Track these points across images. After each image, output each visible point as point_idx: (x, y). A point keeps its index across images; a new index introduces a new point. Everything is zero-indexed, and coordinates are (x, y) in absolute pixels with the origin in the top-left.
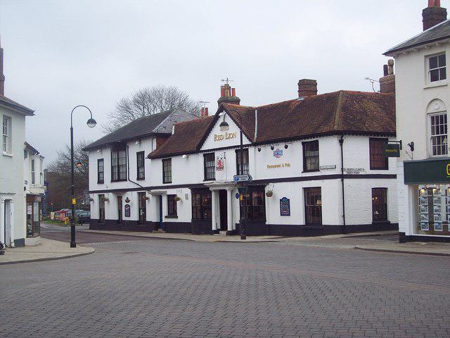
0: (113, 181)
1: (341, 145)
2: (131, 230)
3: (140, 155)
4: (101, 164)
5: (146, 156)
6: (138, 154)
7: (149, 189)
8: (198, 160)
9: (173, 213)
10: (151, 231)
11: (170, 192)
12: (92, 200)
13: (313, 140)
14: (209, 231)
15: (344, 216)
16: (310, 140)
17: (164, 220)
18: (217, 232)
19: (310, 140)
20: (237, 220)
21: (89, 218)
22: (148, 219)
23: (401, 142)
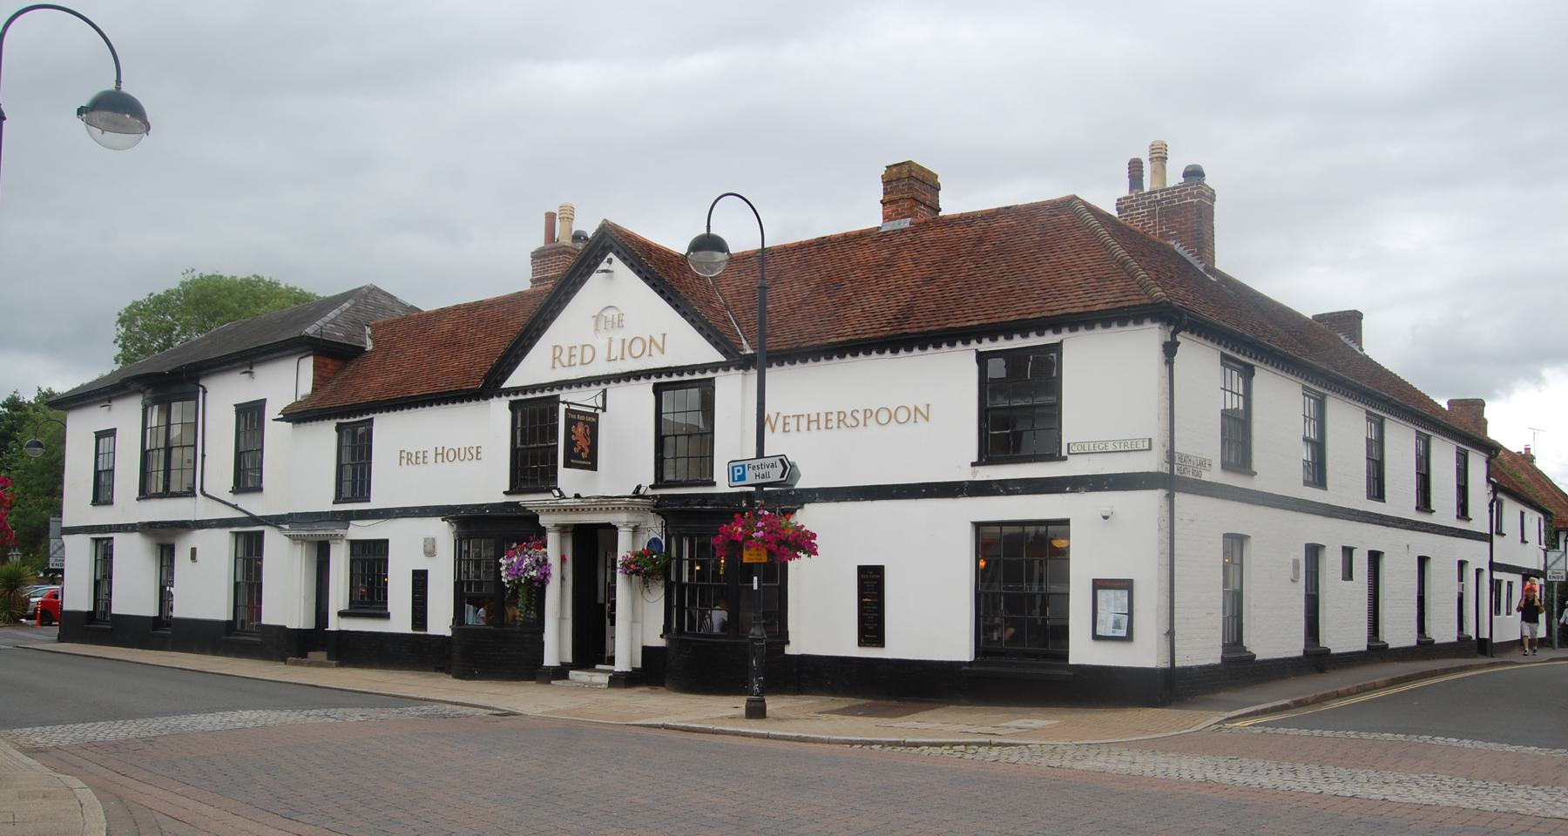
0: (144, 494)
1: (1169, 362)
3: (250, 415)
4: (105, 442)
5: (272, 411)
7: (276, 521)
9: (369, 595)
12: (1201, 263)
13: (1034, 340)
15: (1171, 634)
17: (335, 624)
18: (561, 672)
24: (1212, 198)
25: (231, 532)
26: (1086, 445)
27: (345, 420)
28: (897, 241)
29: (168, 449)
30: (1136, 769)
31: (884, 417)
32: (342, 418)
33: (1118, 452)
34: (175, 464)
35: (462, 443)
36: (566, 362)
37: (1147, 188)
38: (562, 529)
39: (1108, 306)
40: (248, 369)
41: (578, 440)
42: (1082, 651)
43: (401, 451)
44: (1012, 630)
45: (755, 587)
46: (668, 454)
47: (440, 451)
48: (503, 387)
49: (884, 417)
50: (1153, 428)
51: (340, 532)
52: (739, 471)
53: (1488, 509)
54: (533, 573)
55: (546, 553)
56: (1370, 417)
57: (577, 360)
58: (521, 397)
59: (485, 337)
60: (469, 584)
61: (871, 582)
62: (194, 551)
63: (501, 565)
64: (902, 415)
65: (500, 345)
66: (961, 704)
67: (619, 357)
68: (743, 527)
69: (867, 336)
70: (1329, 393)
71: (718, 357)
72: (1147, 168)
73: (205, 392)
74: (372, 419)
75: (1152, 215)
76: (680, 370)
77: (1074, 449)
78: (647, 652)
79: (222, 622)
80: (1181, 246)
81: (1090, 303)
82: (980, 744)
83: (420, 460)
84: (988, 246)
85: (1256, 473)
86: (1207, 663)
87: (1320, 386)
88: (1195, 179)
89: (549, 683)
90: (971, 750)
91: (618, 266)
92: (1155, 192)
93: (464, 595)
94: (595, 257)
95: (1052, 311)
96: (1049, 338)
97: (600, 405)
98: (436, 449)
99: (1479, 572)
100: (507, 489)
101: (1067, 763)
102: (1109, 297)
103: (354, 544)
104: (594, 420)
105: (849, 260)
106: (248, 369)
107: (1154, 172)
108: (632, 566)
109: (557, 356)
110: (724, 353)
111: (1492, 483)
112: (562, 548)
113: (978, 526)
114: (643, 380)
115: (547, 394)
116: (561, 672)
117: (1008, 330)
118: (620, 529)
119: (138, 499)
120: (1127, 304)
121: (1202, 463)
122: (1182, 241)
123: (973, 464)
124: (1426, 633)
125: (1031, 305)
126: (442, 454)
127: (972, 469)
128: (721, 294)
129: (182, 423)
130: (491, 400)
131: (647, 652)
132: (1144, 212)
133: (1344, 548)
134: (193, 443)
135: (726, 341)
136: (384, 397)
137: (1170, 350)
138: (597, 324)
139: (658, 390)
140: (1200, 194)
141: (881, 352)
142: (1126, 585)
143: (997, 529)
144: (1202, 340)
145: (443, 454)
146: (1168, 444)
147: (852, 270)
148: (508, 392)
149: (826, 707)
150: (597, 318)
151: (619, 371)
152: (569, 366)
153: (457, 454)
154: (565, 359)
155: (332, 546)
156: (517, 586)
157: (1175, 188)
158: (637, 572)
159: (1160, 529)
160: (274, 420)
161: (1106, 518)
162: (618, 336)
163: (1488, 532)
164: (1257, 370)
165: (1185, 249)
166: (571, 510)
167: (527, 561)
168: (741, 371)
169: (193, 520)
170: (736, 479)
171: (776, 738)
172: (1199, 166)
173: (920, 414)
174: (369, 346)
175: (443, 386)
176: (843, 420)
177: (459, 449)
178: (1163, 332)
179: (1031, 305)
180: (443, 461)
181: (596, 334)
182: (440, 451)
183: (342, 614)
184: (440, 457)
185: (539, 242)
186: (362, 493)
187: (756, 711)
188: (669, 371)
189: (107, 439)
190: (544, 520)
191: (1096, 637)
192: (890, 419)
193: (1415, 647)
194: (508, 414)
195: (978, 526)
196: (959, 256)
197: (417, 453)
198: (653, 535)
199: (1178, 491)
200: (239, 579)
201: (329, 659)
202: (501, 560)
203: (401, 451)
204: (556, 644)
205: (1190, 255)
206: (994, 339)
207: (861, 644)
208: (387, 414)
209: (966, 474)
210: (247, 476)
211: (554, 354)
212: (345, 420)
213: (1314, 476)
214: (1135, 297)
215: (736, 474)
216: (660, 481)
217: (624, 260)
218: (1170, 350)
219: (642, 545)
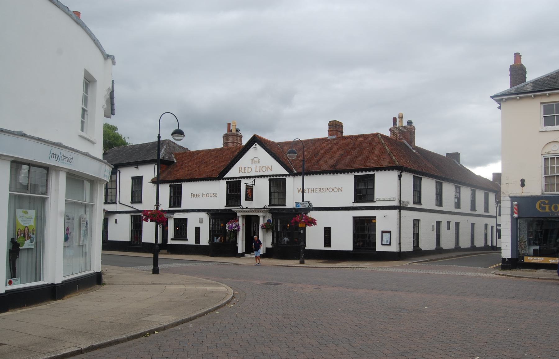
1: (400, 180)
2: (125, 250)
3: (137, 181)
8: (221, 187)
11: (177, 216)
13: (368, 173)
14: (232, 252)
15: (400, 244)
17: (169, 242)
18: (242, 255)
24: (414, 129)
25: (130, 215)
26: (380, 199)
27: (172, 184)
28: (332, 142)
30: (389, 271)
31: (331, 190)
32: (172, 183)
35: (211, 192)
36: (243, 171)
37: (397, 126)
38: (243, 217)
39: (386, 166)
40: (136, 167)
42: (379, 248)
43: (191, 194)
44: (362, 243)
45: (302, 233)
46: (273, 197)
48: (224, 177)
49: (331, 190)
50: (396, 196)
51: (172, 216)
53: (496, 209)
54: (236, 228)
55: (238, 223)
56: (456, 187)
57: (246, 171)
58: (229, 180)
59: (214, 161)
60: (215, 231)
61: (327, 231)
63: (226, 226)
64: (335, 190)
66: (350, 261)
67: (259, 171)
68: (299, 218)
69: (327, 170)
70: (444, 182)
71: (287, 173)
72: (398, 120)
73: (120, 172)
75: (399, 133)
77: (377, 200)
78: (267, 249)
79: (127, 242)
81: (381, 165)
82: (357, 267)
83: (198, 196)
84: (356, 146)
86: (409, 251)
87: (441, 180)
88: (410, 124)
89: (240, 257)
90: (355, 268)
91: (258, 146)
92: (400, 127)
93: (213, 234)
95: (372, 166)
96: (372, 173)
98: (203, 193)
99: (492, 227)
100: (226, 205)
101: (375, 270)
102: (386, 164)
104: (252, 188)
105: (320, 147)
106: (136, 167)
107: (399, 121)
108: (265, 227)
110: (288, 172)
111: (497, 201)
112: (243, 222)
113: (354, 218)
114: (266, 178)
117: (362, 170)
120: (390, 166)
121: (408, 203)
123: (353, 203)
124: (474, 244)
125: (367, 164)
126: (204, 195)
127: (353, 204)
128: (285, 154)
130: (220, 181)
131: (267, 249)
133: (447, 222)
134: (115, 187)
135: (289, 169)
136: (186, 178)
137: (400, 177)
138: (252, 161)
139: (270, 180)
140: (411, 129)
141: (330, 174)
142: (389, 232)
143: (359, 218)
144: (408, 173)
145: (205, 195)
146: (399, 199)
147: (321, 150)
148: (226, 179)
149: (317, 262)
150: (252, 160)
151: (259, 175)
152: (244, 172)
153: (209, 195)
155: (168, 220)
156: (231, 231)
157: (405, 126)
158: (265, 228)
159: (397, 219)
161: (385, 216)
162: (258, 165)
163: (495, 215)
164: (422, 178)
166: (247, 212)
167: (234, 225)
168: (293, 177)
169: (116, 211)
171: (310, 267)
172: (411, 121)
173: (340, 190)
174: (175, 161)
175: (204, 176)
178: (398, 172)
179: (367, 164)
183: (172, 239)
184: (204, 196)
185: (226, 132)
186: (178, 203)
187: (302, 262)
188: (273, 176)
190: (238, 214)
191: (382, 244)
192: (332, 191)
193: (470, 248)
194: (226, 184)
195: (354, 218)
196: (349, 148)
198: (269, 218)
199: (402, 210)
200: (132, 229)
201: (168, 252)
202: (226, 225)
203: (191, 194)
204: (241, 246)
206: (358, 172)
207: (325, 247)
208: (187, 183)
209: (351, 205)
210: (136, 197)
212: (172, 184)
213: (439, 203)
214: (392, 164)
215: (297, 206)
216: (270, 204)
217: (260, 145)
218: (400, 177)
219: (266, 222)
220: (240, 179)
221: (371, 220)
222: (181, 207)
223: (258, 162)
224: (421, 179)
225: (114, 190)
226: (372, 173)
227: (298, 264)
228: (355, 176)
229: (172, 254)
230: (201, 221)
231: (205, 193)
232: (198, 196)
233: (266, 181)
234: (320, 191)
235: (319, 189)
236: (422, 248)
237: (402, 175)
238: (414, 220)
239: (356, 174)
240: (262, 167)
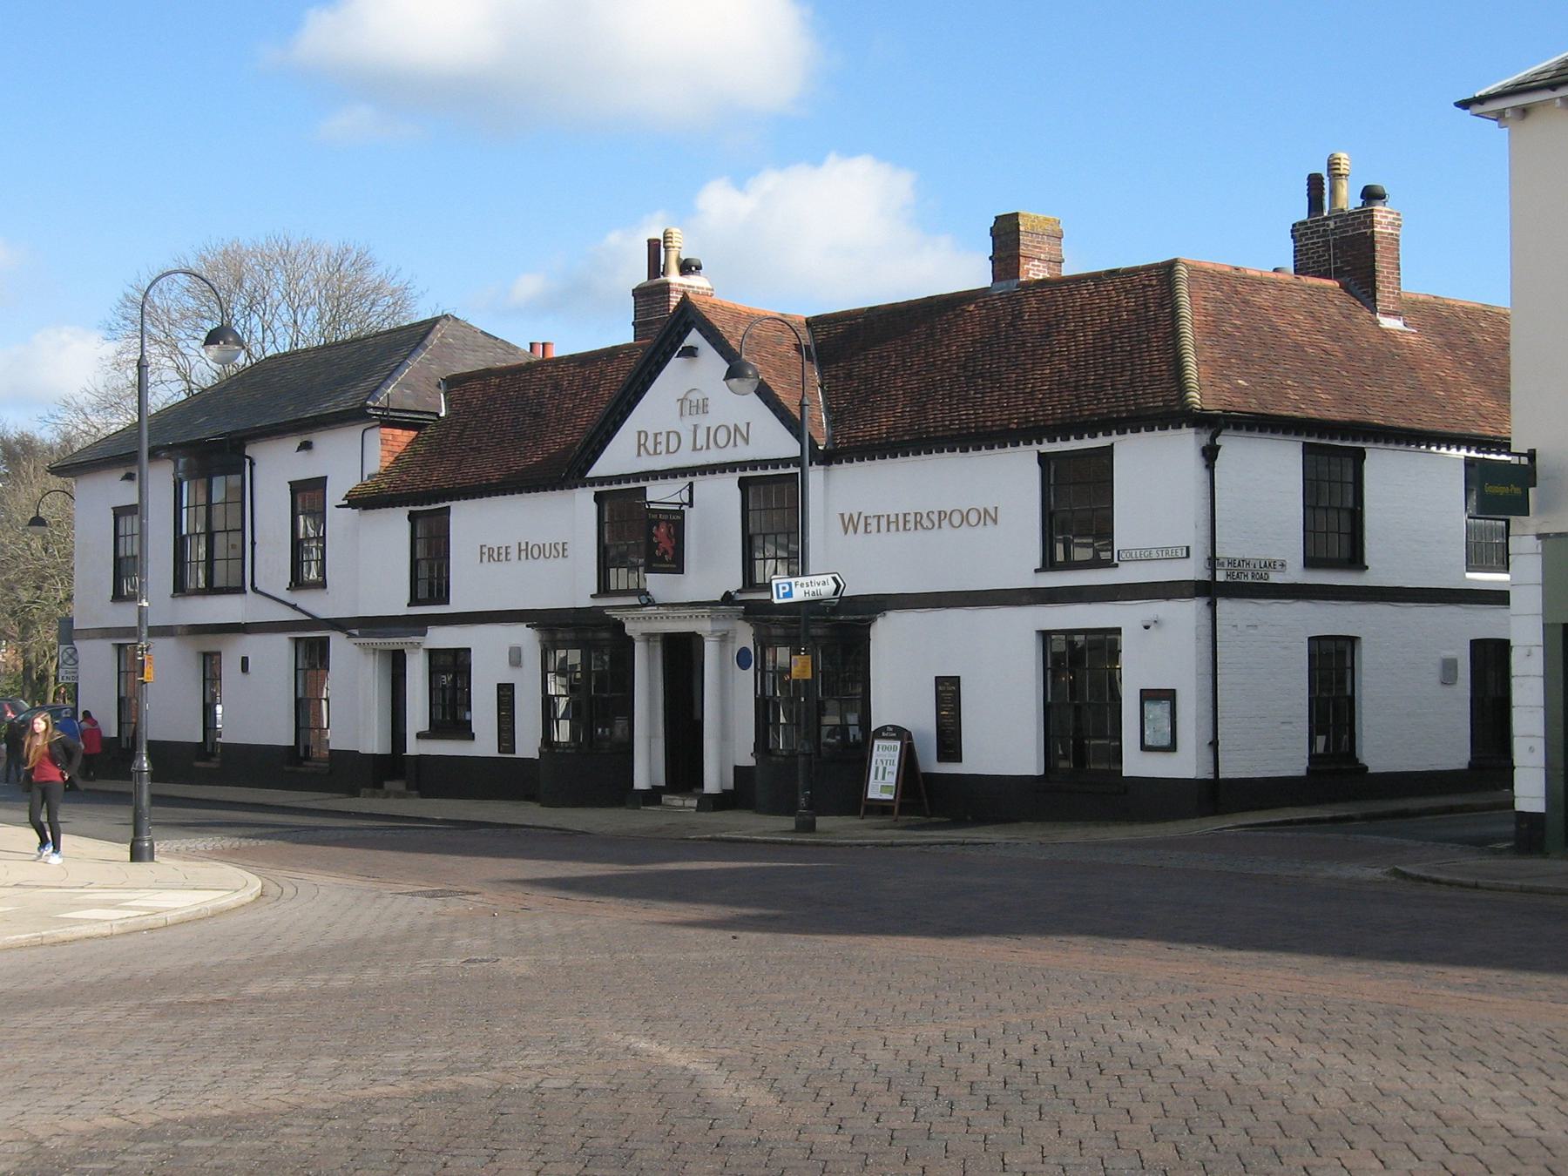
3: (308, 494)
4: (129, 524)
5: (335, 494)
6: (297, 488)
10: (354, 793)
11: (442, 638)
13: (1087, 443)
15: (1214, 744)
16: (1073, 445)
17: (413, 747)
19: (1073, 445)
20: (745, 756)
21: (824, 715)
22: (1218, 579)
23: (1532, 455)
25: (290, 638)
26: (1154, 551)
29: (210, 536)
31: (956, 519)
33: (1160, 559)
34: (219, 552)
35: (546, 539)
36: (651, 451)
41: (659, 543)
42: (1135, 764)
47: (523, 547)
48: (587, 476)
49: (956, 519)
50: (1194, 537)
52: (784, 588)
58: (605, 488)
62: (245, 661)
64: (973, 518)
65: (588, 416)
67: (705, 447)
73: (252, 464)
74: (449, 507)
76: (764, 464)
80: (1356, 284)
83: (503, 557)
85: (1367, 568)
94: (635, 393)
96: (1101, 441)
97: (687, 501)
98: (520, 544)
103: (433, 654)
104: (679, 517)
109: (642, 442)
114: (728, 474)
115: (633, 485)
116: (652, 796)
118: (706, 639)
119: (173, 596)
122: (1357, 279)
123: (1036, 571)
126: (525, 551)
129: (226, 503)
132: (1319, 242)
137: (1210, 454)
139: (743, 483)
142: (1169, 696)
150: (682, 401)
153: (542, 549)
154: (650, 445)
160: (337, 507)
161: (1147, 627)
165: (1359, 289)
168: (822, 467)
170: (781, 596)
173: (989, 517)
176: (920, 522)
177: (544, 545)
180: (527, 558)
181: (681, 419)
182: (523, 547)
183: (420, 736)
184: (524, 554)
188: (754, 464)
189: (129, 518)
190: (630, 628)
194: (594, 507)
195: (1045, 636)
197: (499, 548)
203: (481, 547)
205: (1364, 295)
211: (639, 441)
215: (781, 592)
218: (1210, 454)
220: (642, 484)
221: (1106, 643)
222: (448, 603)
223: (700, 411)
224: (1360, 456)
225: (235, 538)
226: (1101, 441)
227: (792, 831)
228: (1043, 459)
229: (424, 795)
230: (515, 658)
231: (527, 543)
232: (503, 557)
233: (728, 487)
234: (918, 525)
235: (916, 514)
236: (1367, 764)
237: (1219, 447)
238: (1310, 639)
239: (1047, 447)
240: (717, 430)
